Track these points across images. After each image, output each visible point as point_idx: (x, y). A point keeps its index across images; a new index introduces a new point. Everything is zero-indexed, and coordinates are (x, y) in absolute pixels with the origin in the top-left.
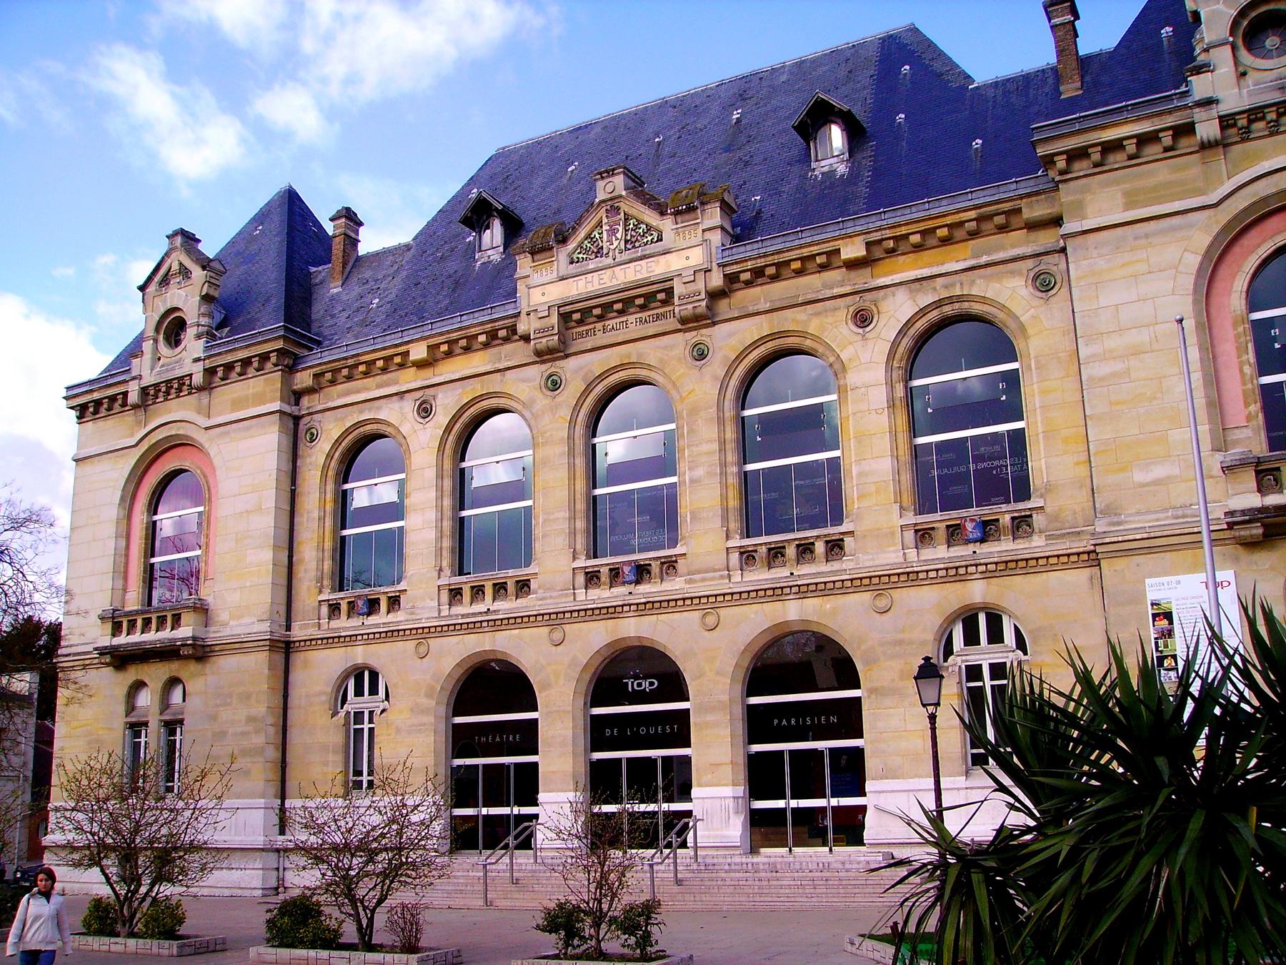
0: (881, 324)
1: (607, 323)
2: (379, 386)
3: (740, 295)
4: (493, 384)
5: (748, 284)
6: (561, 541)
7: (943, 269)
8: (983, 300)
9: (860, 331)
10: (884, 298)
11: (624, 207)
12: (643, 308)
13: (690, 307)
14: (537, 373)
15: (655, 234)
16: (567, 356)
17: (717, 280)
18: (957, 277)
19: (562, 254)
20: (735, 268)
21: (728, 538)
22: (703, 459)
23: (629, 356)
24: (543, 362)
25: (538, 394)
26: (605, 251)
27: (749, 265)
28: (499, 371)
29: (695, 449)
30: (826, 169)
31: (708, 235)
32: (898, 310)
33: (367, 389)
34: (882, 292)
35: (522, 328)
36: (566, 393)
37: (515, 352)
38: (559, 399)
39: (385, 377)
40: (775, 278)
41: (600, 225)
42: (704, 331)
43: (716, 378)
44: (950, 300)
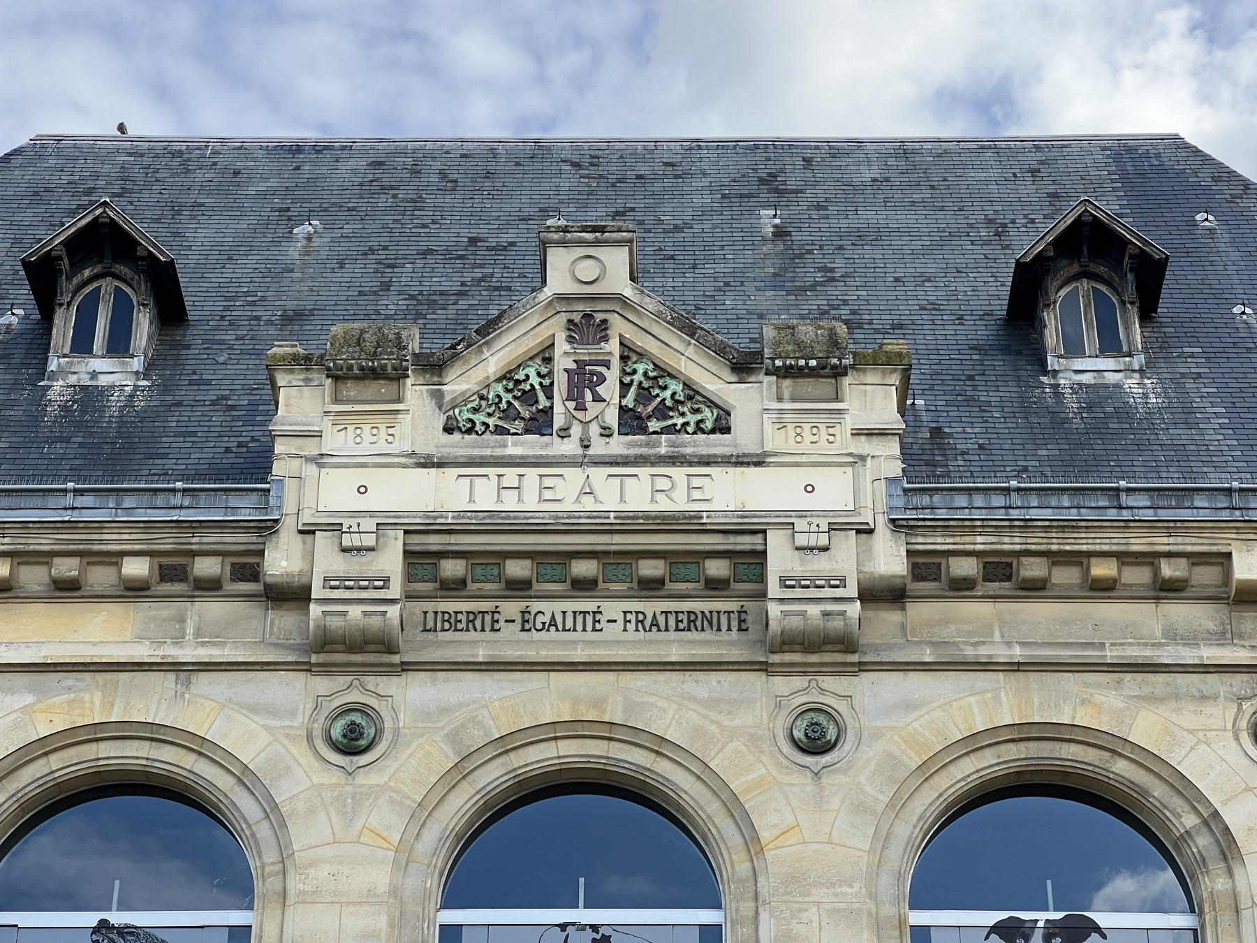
1: (536, 606)
3: (918, 611)
4: (613, 697)
5: (962, 587)
11: (619, 327)
12: (651, 587)
13: (814, 610)
14: (302, 697)
15: (709, 416)
17: (889, 559)
19: (417, 414)
20: (939, 542)
23: (598, 703)
24: (326, 669)
26: (558, 421)
27: (981, 542)
28: (175, 667)
30: (1086, 378)
35: (281, 561)
36: (391, 766)
37: (218, 626)
38: (362, 779)
40: (1035, 589)
41: (545, 355)
42: (829, 682)
43: (860, 808)
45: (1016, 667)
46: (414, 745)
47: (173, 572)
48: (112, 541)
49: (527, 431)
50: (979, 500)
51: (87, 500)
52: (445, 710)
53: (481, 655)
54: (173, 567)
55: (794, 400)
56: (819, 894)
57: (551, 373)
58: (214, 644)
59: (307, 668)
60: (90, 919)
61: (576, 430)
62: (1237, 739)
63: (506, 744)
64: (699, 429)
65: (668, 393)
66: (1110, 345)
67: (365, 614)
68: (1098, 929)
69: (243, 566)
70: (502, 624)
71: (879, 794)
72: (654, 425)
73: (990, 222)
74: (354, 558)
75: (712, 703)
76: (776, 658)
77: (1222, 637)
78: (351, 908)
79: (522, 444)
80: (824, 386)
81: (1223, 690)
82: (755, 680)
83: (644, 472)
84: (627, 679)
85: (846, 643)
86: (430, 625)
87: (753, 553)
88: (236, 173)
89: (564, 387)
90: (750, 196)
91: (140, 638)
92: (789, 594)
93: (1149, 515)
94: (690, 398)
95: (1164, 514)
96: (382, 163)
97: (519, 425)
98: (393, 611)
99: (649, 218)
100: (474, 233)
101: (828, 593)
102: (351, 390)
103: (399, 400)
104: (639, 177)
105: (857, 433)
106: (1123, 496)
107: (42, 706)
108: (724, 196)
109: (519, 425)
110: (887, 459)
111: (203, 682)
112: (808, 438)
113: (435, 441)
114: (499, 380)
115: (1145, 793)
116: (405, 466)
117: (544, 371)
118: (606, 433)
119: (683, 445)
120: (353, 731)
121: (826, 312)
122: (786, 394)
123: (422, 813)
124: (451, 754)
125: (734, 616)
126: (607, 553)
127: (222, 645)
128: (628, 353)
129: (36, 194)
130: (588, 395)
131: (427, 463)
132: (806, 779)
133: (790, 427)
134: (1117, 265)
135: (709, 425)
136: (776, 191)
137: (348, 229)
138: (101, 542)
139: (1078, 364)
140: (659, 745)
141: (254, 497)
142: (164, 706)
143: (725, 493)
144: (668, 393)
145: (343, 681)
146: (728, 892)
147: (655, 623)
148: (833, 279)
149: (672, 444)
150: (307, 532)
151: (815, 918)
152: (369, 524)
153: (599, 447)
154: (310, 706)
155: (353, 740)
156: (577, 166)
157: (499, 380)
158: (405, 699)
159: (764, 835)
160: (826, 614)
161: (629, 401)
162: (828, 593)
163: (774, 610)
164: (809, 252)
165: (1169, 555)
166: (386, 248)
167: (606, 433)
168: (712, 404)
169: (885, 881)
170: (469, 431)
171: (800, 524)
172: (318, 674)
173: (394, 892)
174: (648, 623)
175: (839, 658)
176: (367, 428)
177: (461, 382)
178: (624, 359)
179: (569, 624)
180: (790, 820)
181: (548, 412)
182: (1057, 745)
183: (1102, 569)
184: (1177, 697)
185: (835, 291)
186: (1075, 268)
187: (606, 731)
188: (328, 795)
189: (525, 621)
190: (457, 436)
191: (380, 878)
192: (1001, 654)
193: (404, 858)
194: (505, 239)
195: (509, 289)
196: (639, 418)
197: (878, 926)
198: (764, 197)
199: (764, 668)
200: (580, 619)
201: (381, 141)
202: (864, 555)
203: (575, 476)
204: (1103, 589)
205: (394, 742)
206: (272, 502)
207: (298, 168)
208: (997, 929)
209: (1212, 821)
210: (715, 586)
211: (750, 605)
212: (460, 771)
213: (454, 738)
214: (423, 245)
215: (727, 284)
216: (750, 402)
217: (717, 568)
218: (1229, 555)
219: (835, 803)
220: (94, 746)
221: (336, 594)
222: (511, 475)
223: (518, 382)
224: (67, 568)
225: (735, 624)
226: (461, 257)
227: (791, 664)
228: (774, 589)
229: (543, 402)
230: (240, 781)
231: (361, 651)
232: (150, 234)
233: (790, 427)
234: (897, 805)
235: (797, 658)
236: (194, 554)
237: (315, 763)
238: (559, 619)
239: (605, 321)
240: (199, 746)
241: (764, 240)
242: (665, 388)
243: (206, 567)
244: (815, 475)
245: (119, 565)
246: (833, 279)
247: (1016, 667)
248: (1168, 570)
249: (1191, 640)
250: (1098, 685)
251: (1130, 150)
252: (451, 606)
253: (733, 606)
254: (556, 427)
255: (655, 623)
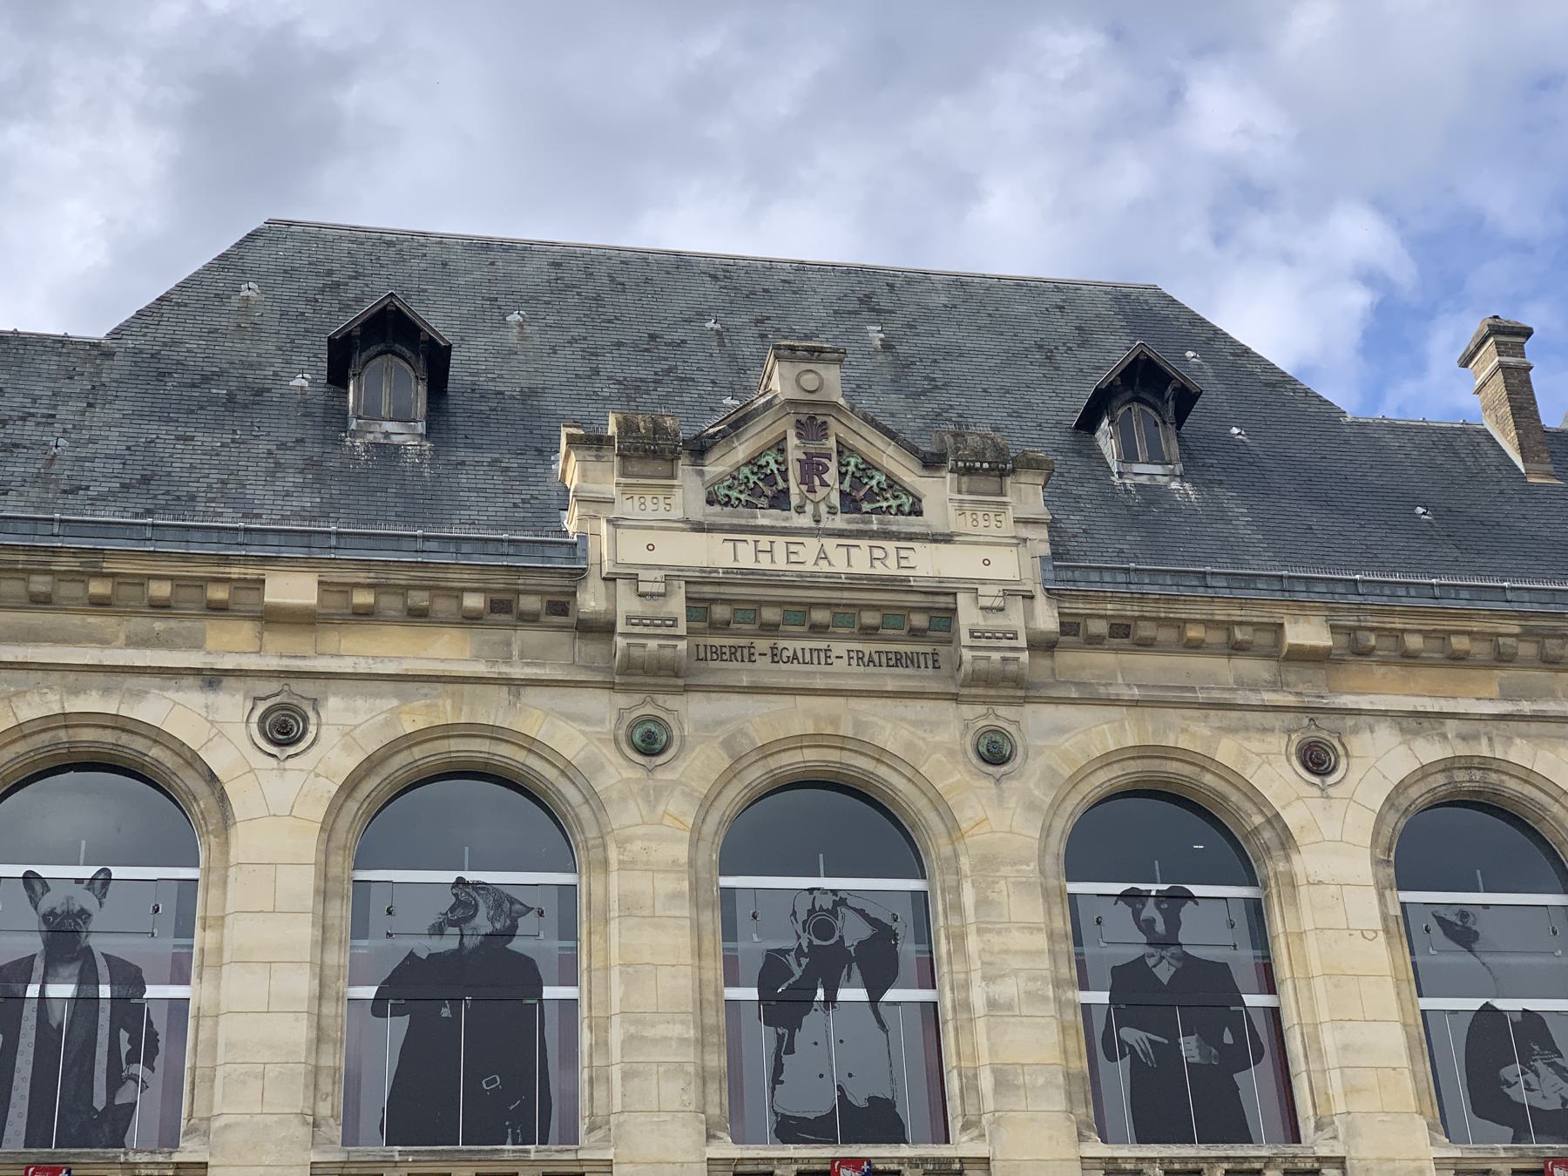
0: (1353, 777)
1: (782, 644)
2: (134, 642)
3: (1068, 659)
4: (844, 715)
5: (1094, 642)
6: (676, 1093)
7: (1461, 706)
8: (1528, 777)
9: (1316, 780)
10: (1355, 730)
11: (835, 427)
12: (868, 632)
13: (996, 656)
14: (606, 710)
15: (906, 502)
16: (687, 689)
17: (1046, 619)
18: (1480, 726)
19: (687, 491)
20: (1081, 607)
21: (710, 1137)
22: (1015, 963)
23: (834, 721)
24: (626, 689)
25: (609, 754)
26: (795, 500)
27: (1110, 608)
29: (996, 941)
30: (1143, 480)
31: (1024, 532)
32: (346, 732)
33: (104, 642)
34: (1350, 721)
35: (591, 601)
36: (681, 766)
37: (536, 650)
38: (663, 776)
39: (159, 625)
40: (1146, 645)
41: (780, 446)
42: (1002, 711)
43: (1031, 806)
44: (1467, 763)
45: (1135, 703)
46: (697, 750)
47: (502, 607)
48: (456, 578)
49: (771, 507)
50: (1107, 577)
51: (433, 545)
52: (719, 723)
53: (745, 681)
54: (502, 602)
55: (970, 492)
56: (1006, 870)
57: (785, 462)
58: (535, 665)
59: (611, 686)
60: (450, 877)
61: (809, 508)
62: (1288, 760)
63: (766, 751)
64: (900, 511)
65: (874, 483)
66: (1156, 457)
67: (660, 646)
68: (1192, 897)
69: (557, 603)
70: (757, 657)
71: (1045, 797)
72: (866, 507)
73: (1040, 347)
74: (648, 602)
75: (917, 724)
76: (965, 691)
77: (1277, 685)
78: (662, 875)
79: (770, 516)
80: (991, 483)
81: (1278, 724)
82: (949, 707)
83: (864, 543)
84: (854, 703)
85: (1018, 681)
86: (702, 655)
87: (947, 609)
88: (445, 264)
89: (798, 473)
90: (855, 313)
91: (476, 658)
92: (977, 643)
93: (1226, 593)
94: (890, 487)
95: (1237, 593)
96: (560, 265)
97: (764, 502)
98: (682, 645)
99: (782, 326)
100: (651, 330)
101: (1005, 643)
102: (635, 467)
103: (673, 477)
104: (766, 291)
105: (1017, 521)
106: (1209, 578)
107: (406, 708)
108: (836, 312)
109: (764, 502)
110: (1039, 539)
111: (530, 694)
112: (982, 523)
113: (699, 510)
114: (746, 465)
115: (1225, 798)
116: (683, 530)
117: (780, 459)
118: (832, 511)
119: (889, 523)
120: (649, 737)
121: (939, 415)
122: (964, 488)
123: (707, 804)
124: (725, 756)
125: (929, 657)
126: (838, 605)
127: (542, 665)
128: (842, 448)
129: (285, 272)
130: (817, 481)
131: (699, 528)
132: (988, 784)
133: (968, 513)
134: (1160, 394)
135: (907, 508)
136: (873, 310)
137: (550, 320)
138: (447, 580)
139: (1137, 468)
140: (880, 755)
141: (565, 549)
142: (500, 713)
143: (927, 563)
144: (874, 483)
145: (638, 698)
146: (931, 864)
147: (871, 660)
148: (936, 387)
149: (881, 522)
150: (610, 579)
151: (1004, 888)
152: (994, 590)
153: (828, 523)
154: (615, 717)
155: (650, 743)
156: (714, 277)
157: (746, 465)
158: (690, 713)
159: (964, 826)
160: (1004, 659)
161: (846, 487)
162: (1005, 643)
163: (967, 655)
164: (913, 363)
165: (1240, 623)
166: (585, 339)
167: (832, 511)
168: (908, 493)
169: (1049, 860)
170: (726, 504)
171: (982, 590)
172: (620, 691)
173: (692, 863)
174: (866, 659)
175: (1011, 692)
176: (649, 498)
177: (719, 465)
178: (840, 453)
179: (808, 659)
180: (982, 815)
181: (786, 492)
182: (1164, 762)
183: (1194, 633)
184: (1247, 729)
185: (942, 398)
186: (1129, 395)
187: (840, 742)
188: (635, 788)
189: (774, 655)
190: (717, 508)
191: (681, 852)
192: (1126, 693)
193: (695, 841)
194: (678, 335)
195: (693, 380)
196: (854, 501)
197: (1046, 893)
198: (866, 314)
199: (955, 698)
200: (815, 654)
201: (553, 244)
202: (1029, 615)
203: (812, 544)
204: (1195, 647)
205: (681, 748)
206: (579, 553)
207: (492, 264)
208: (1123, 896)
209: (1275, 820)
210: (916, 634)
211: (942, 650)
212: (731, 774)
213: (727, 745)
214: (615, 337)
215: (859, 386)
216: (939, 495)
217: (919, 620)
218: (1282, 625)
219: (1012, 802)
220: (446, 742)
221: (637, 630)
222: (764, 542)
223: (760, 467)
224: (419, 599)
225: (930, 663)
226: (647, 350)
227: (975, 696)
228: (965, 639)
229: (781, 485)
230: (563, 773)
231: (655, 675)
232: (437, 319)
233: (968, 513)
234: (1056, 806)
235: (980, 691)
236: (519, 592)
237: (621, 760)
238: (800, 654)
239: (825, 423)
240: (530, 745)
241: (876, 350)
242: (872, 478)
243: (530, 603)
244: (983, 552)
245: (460, 599)
246: (936, 387)
247: (1135, 703)
248: (1239, 634)
249: (1254, 687)
250: (1192, 718)
251: (1127, 296)
252: (717, 641)
253: (929, 649)
254: (793, 504)
255: (871, 660)
